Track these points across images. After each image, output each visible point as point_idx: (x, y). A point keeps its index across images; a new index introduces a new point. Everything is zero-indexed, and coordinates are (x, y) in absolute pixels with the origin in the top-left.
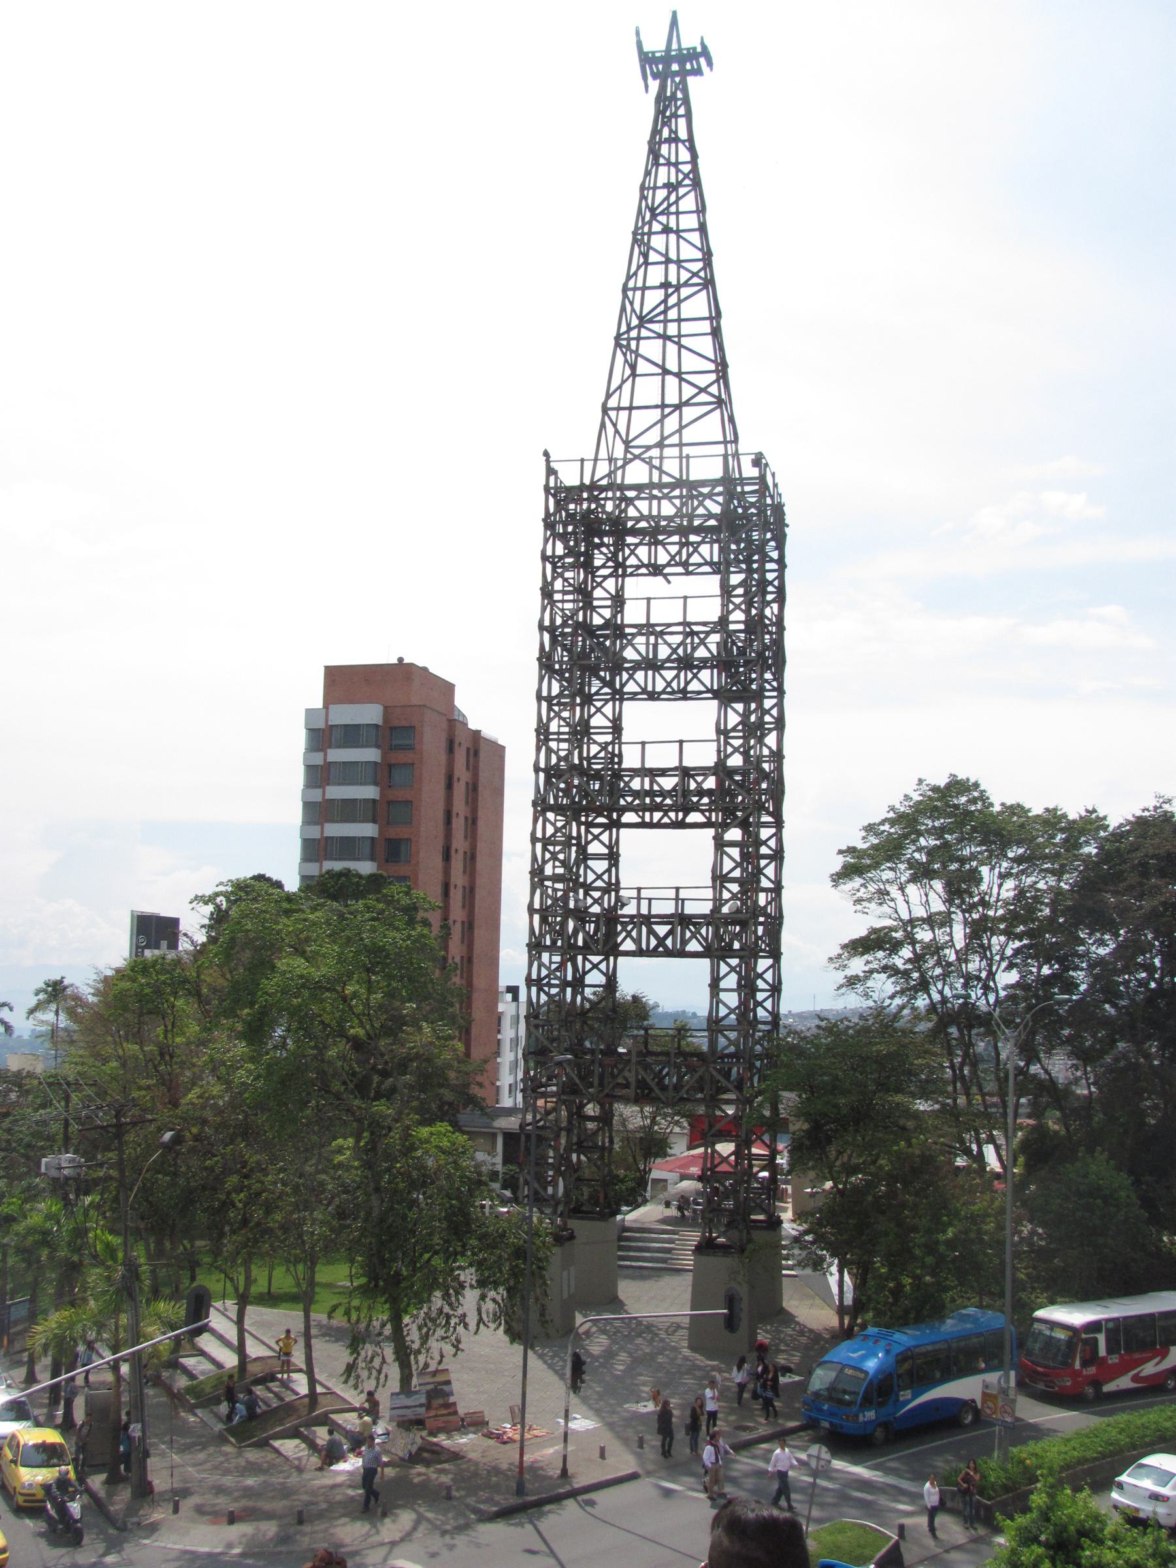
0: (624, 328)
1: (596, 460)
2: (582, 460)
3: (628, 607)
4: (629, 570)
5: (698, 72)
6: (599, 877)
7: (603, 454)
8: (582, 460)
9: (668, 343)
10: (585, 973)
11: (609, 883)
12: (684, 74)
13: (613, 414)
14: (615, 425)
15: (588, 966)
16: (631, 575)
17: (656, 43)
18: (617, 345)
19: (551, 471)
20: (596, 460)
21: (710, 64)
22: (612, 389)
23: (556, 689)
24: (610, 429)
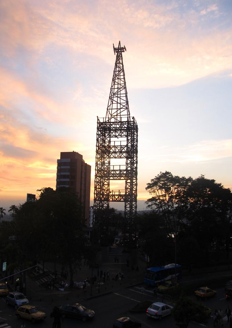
0: (111, 95)
2: (104, 118)
5: (124, 51)
7: (107, 117)
8: (104, 118)
11: (108, 189)
12: (121, 52)
14: (109, 112)
17: (116, 46)
19: (98, 120)
20: (106, 118)
21: (126, 50)
22: (109, 106)
24: (108, 112)
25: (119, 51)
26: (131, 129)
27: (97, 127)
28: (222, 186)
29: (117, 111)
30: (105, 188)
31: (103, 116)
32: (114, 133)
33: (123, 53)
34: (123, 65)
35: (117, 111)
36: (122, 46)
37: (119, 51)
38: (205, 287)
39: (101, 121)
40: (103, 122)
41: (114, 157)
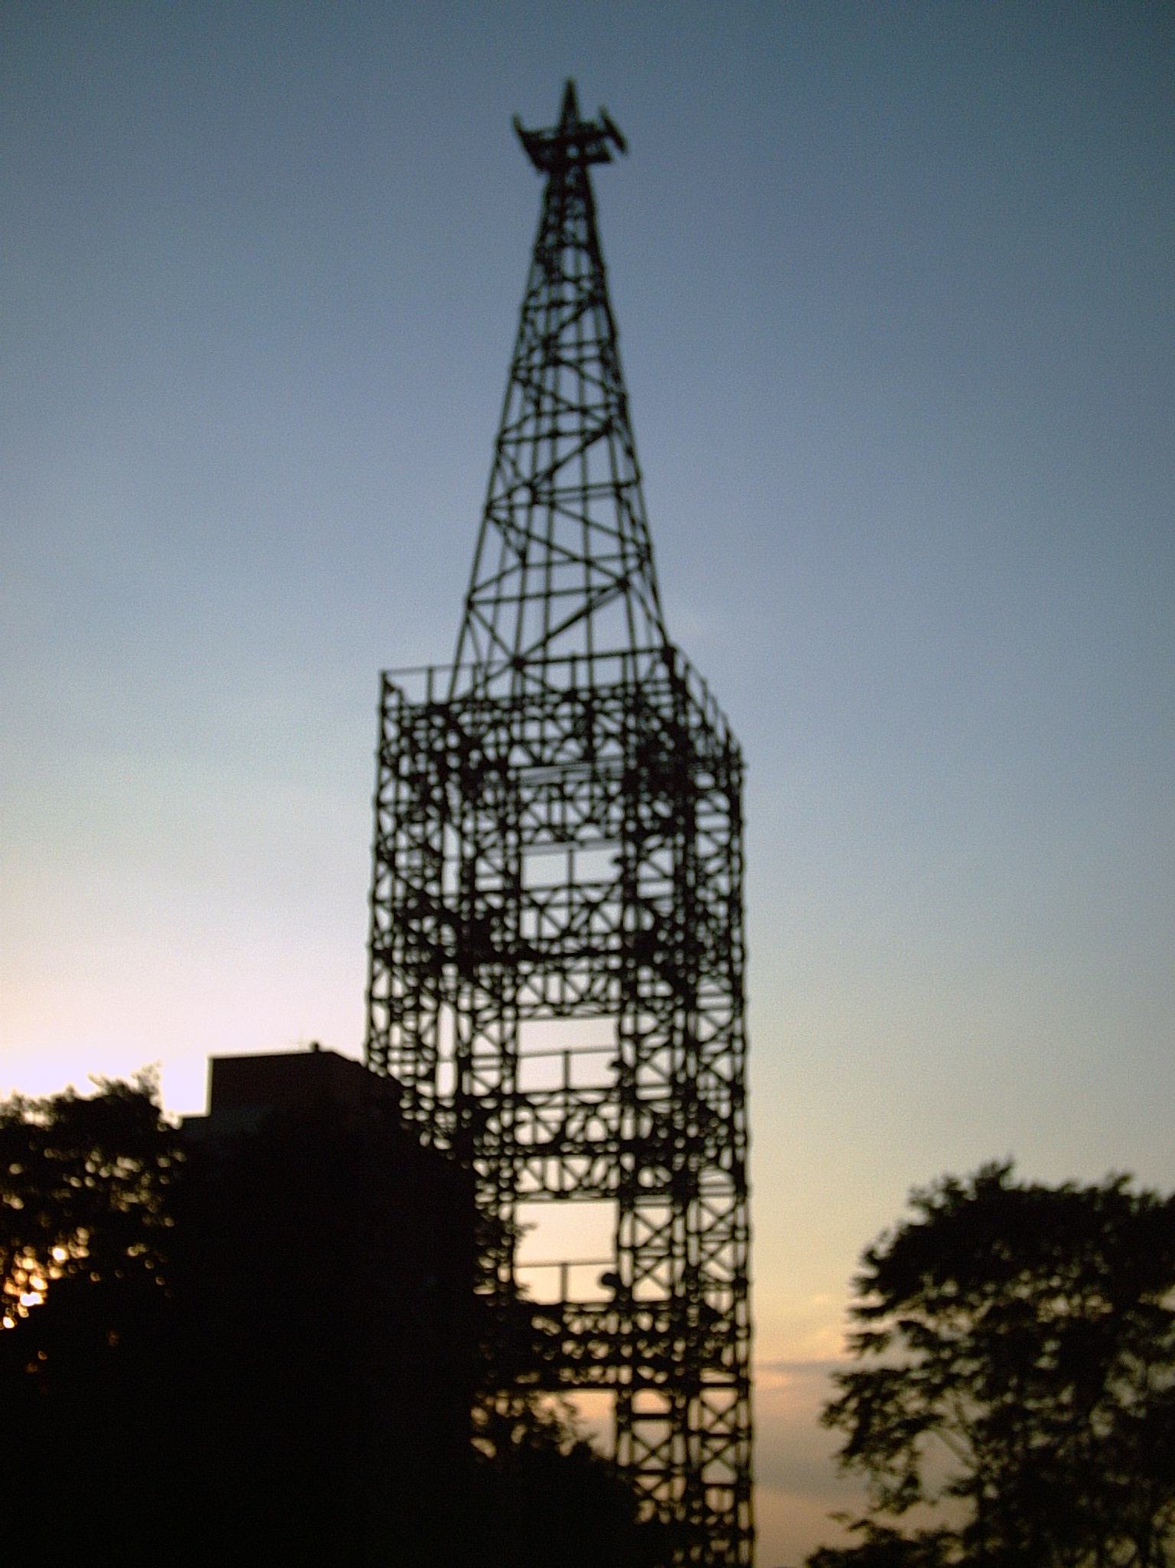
0: (523, 352)
1: (456, 667)
2: (431, 671)
3: (525, 1067)
4: (524, 1012)
5: (604, 158)
6: (653, 1452)
7: (469, 657)
8: (431, 671)
9: (578, 551)
10: (703, 1464)
11: (736, 1429)
12: (584, 161)
13: (487, 612)
14: (492, 630)
15: (707, 1455)
16: (530, 1017)
17: (545, 119)
18: (514, 378)
19: (387, 688)
20: (456, 667)
21: (621, 144)
22: (482, 579)
23: (399, 989)
24: (508, 470)
25: (568, 154)
26: (671, 766)
27: (365, 937)
28: (927, 1206)
29: (544, 644)
30: (709, 1417)
31: (429, 656)
32: (540, 810)
33: (597, 173)
34: (597, 260)
35: (544, 644)
36: (588, 113)
37: (568, 154)
38: (51, 1160)
39: (416, 695)
40: (432, 708)
41: (545, 1002)
